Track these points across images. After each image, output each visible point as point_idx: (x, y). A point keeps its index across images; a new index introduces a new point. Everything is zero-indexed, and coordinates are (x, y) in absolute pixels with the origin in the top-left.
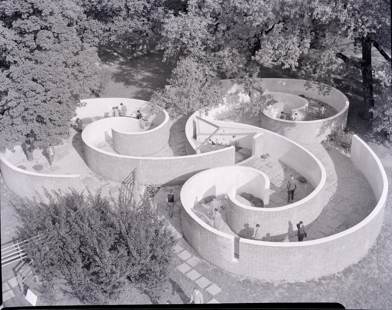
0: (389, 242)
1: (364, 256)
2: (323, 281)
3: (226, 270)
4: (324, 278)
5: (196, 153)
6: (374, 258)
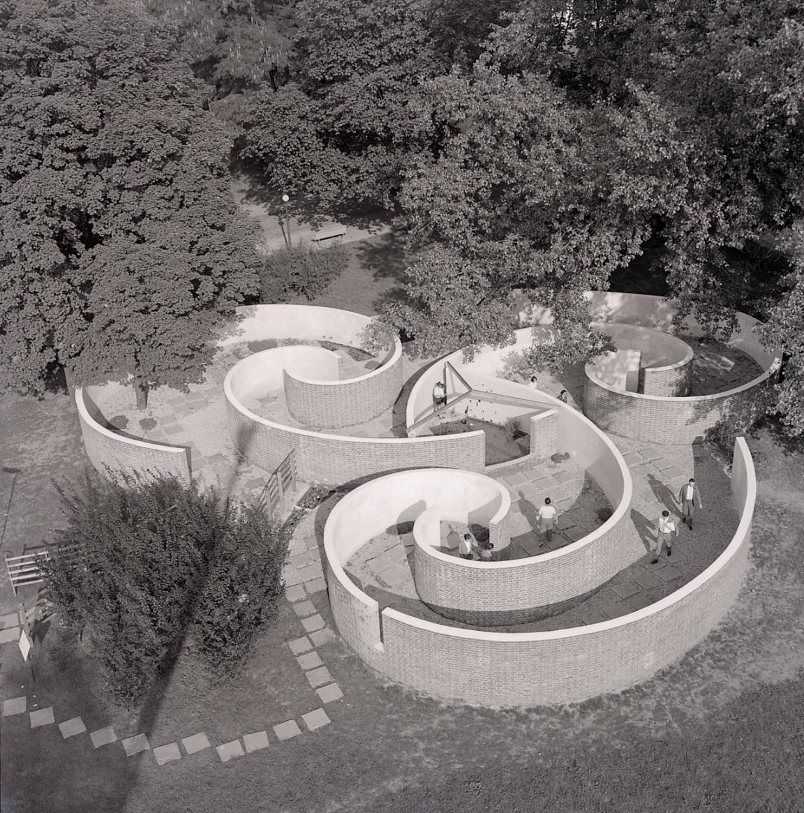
0: (708, 663)
1: (640, 683)
2: (534, 714)
3: (367, 662)
4: (538, 710)
5: (406, 436)
6: (659, 690)
